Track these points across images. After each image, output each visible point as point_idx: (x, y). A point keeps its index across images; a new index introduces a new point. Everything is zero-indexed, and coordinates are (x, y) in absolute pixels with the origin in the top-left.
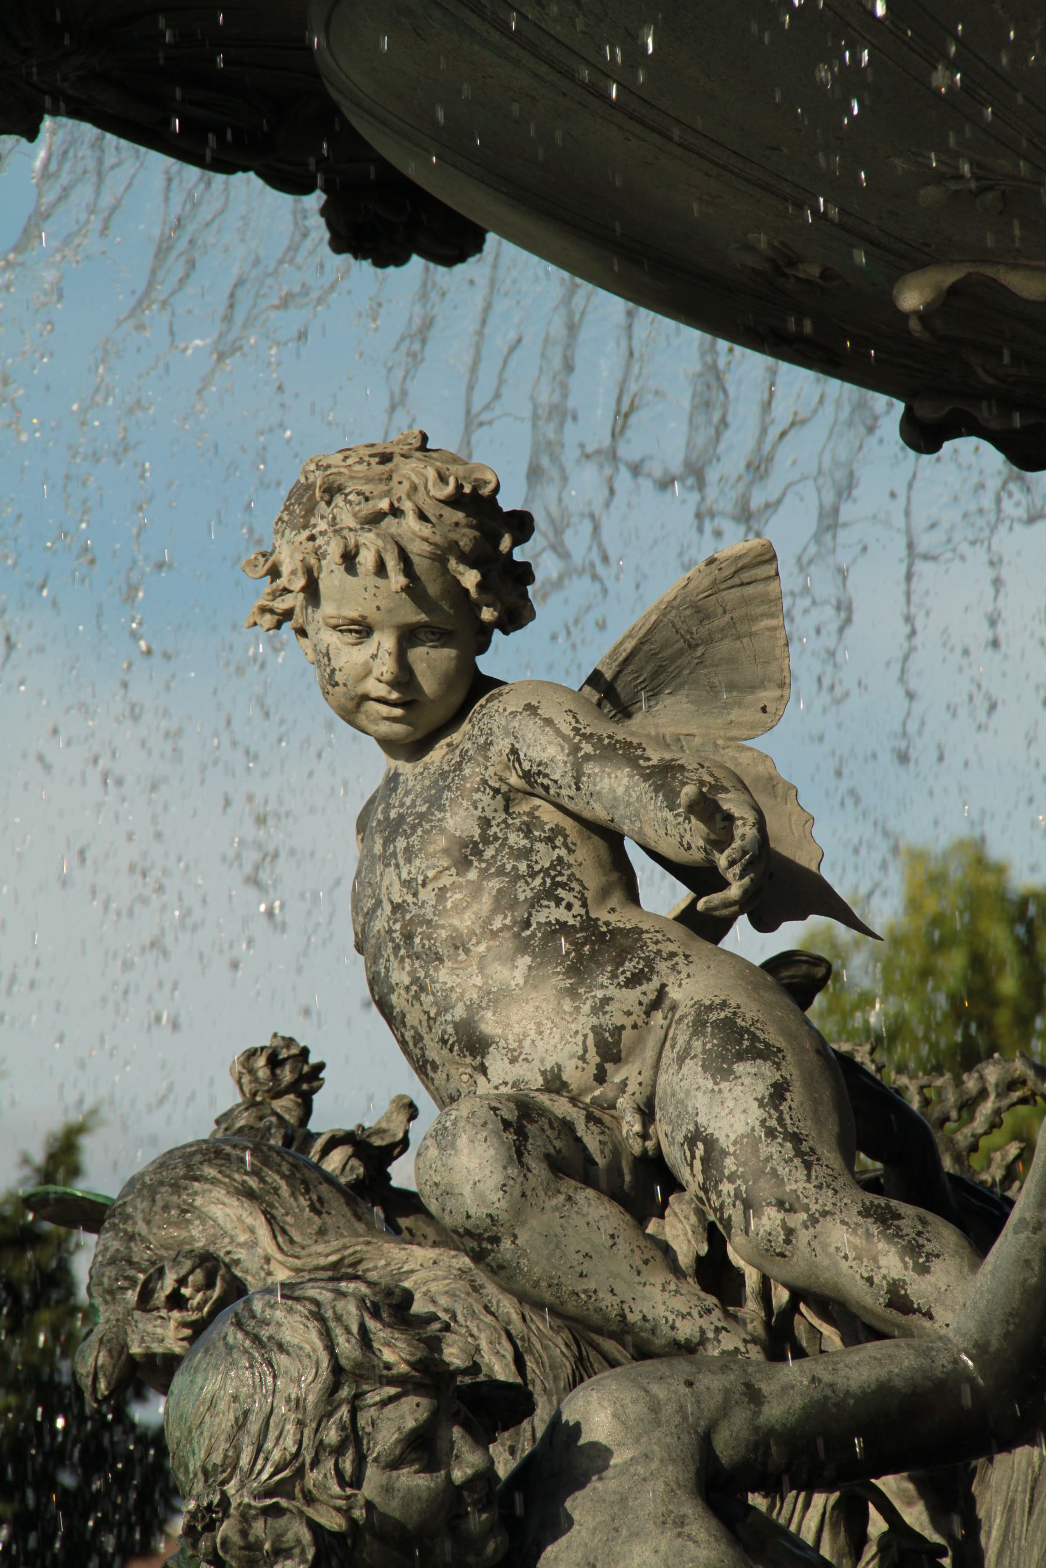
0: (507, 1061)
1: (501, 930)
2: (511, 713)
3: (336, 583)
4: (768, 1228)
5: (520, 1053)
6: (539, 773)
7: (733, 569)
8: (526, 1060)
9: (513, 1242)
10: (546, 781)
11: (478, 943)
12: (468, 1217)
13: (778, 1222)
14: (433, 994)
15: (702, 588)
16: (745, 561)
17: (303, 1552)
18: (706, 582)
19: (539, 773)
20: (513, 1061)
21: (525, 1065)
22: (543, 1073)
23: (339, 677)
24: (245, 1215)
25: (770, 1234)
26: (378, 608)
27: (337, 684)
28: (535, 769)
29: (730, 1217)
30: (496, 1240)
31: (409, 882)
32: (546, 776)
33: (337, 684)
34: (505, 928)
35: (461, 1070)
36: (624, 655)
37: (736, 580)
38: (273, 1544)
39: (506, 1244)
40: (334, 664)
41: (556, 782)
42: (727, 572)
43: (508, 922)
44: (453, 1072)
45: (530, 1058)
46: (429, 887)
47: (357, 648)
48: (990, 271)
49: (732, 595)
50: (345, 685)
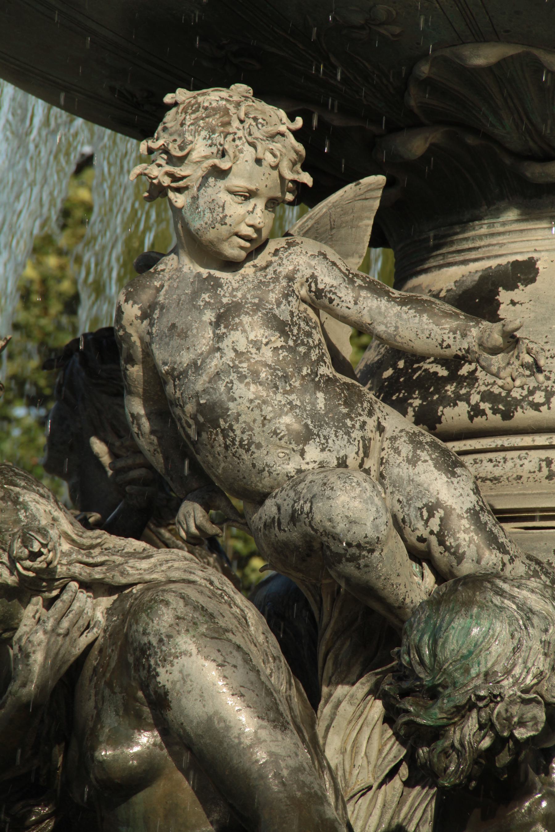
0: (319, 450)
1: (306, 375)
2: (312, 255)
3: (248, 168)
4: (495, 562)
5: (327, 446)
6: (331, 291)
7: (366, 190)
8: (329, 450)
9: (380, 554)
10: (333, 297)
11: (296, 381)
12: (366, 537)
13: (500, 559)
14: (272, 406)
15: (349, 197)
16: (373, 186)
17: (536, 724)
18: (352, 195)
19: (331, 291)
20: (323, 450)
21: (329, 453)
22: (338, 459)
23: (228, 220)
24: (53, 511)
25: (495, 565)
26: (266, 186)
27: (226, 224)
28: (328, 288)
29: (464, 553)
30: (372, 551)
31: (256, 342)
32: (335, 293)
33: (226, 224)
34: (308, 374)
35: (280, 450)
36: (307, 228)
37: (363, 197)
38: (519, 719)
39: (376, 554)
40: (227, 212)
41: (340, 298)
42: (362, 192)
43: (309, 371)
44: (272, 451)
45: (332, 450)
46: (269, 346)
47: (240, 205)
48: (536, 52)
49: (359, 204)
50: (230, 225)
